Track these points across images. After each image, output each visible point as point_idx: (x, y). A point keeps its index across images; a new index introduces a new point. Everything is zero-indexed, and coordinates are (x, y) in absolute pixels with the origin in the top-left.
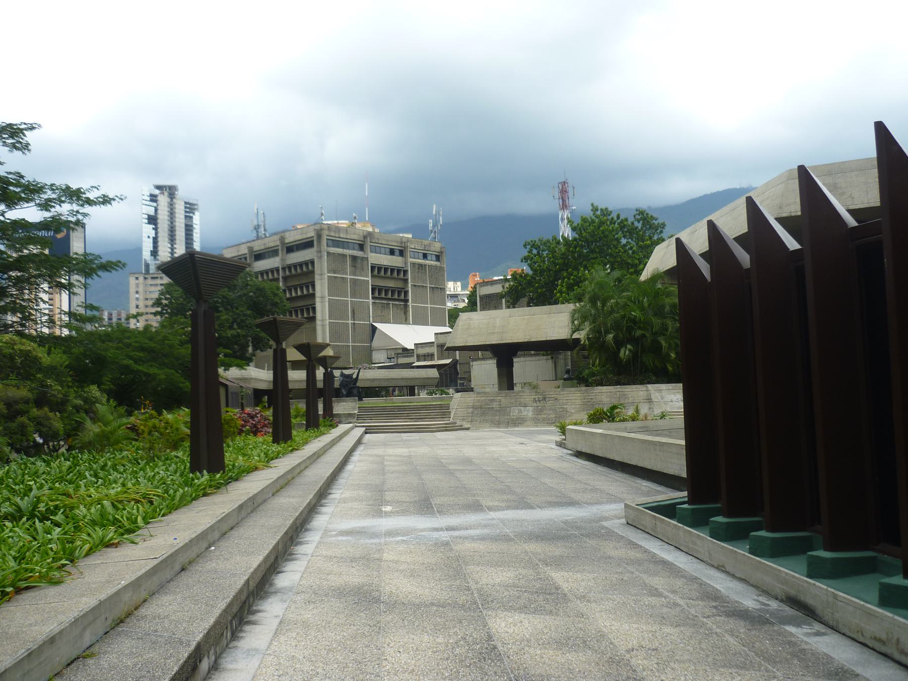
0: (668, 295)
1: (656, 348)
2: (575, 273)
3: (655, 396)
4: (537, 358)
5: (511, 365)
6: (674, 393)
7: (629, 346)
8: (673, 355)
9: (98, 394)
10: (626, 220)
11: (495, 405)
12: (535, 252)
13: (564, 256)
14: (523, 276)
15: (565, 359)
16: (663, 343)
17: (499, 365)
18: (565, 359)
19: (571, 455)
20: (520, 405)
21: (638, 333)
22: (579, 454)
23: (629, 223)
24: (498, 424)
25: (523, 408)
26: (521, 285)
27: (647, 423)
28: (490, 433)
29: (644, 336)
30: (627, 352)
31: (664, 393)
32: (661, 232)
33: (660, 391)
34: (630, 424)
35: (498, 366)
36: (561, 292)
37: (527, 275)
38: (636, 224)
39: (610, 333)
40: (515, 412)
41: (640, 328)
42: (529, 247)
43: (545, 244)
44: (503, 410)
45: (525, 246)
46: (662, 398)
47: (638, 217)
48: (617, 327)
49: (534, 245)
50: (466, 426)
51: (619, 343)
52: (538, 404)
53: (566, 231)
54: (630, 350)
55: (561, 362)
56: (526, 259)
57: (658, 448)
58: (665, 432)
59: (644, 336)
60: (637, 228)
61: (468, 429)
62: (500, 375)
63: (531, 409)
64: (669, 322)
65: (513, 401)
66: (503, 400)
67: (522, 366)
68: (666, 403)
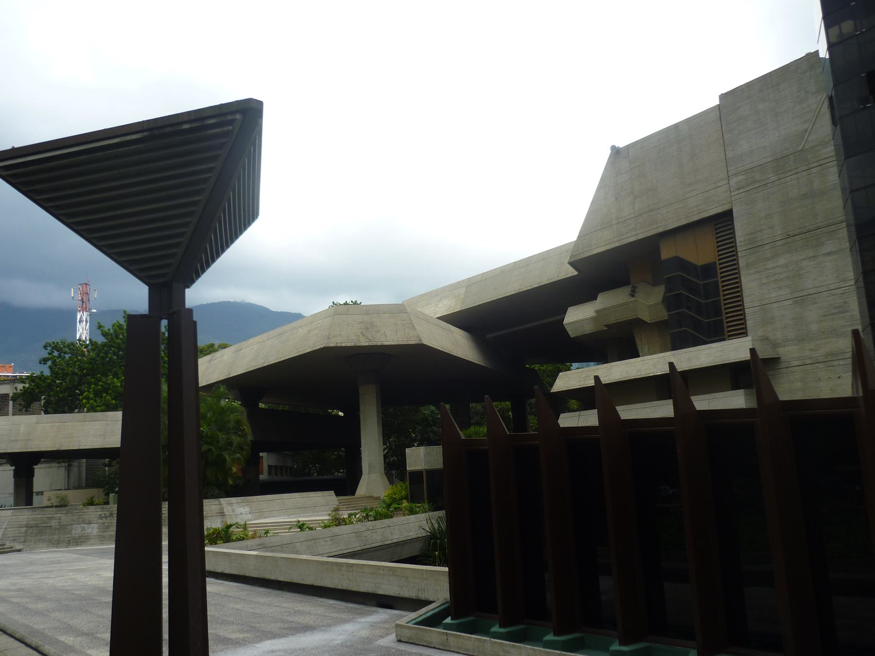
0: (233, 410)
1: (220, 463)
2: (104, 379)
3: (227, 510)
4: (48, 465)
5: (31, 474)
8: (234, 470)
11: (54, 523)
12: (56, 353)
13: (92, 361)
14: (41, 378)
15: (79, 467)
16: (227, 458)
17: (16, 475)
18: (79, 467)
20: (84, 522)
24: (57, 544)
25: (86, 526)
26: (38, 388)
27: (265, 540)
28: (49, 555)
29: (210, 450)
31: (235, 507)
33: (231, 504)
35: (14, 477)
36: (88, 398)
37: (47, 378)
40: (77, 530)
42: (49, 348)
43: (68, 346)
44: (62, 528)
45: (45, 347)
46: (233, 511)
49: (55, 347)
50: (18, 547)
52: (104, 520)
53: (83, 332)
55: (75, 470)
56: (44, 361)
57: (344, 568)
58: (278, 548)
59: (210, 450)
61: (19, 551)
62: (17, 486)
63: (96, 526)
65: (74, 518)
66: (64, 517)
67: (44, 477)
68: (236, 516)
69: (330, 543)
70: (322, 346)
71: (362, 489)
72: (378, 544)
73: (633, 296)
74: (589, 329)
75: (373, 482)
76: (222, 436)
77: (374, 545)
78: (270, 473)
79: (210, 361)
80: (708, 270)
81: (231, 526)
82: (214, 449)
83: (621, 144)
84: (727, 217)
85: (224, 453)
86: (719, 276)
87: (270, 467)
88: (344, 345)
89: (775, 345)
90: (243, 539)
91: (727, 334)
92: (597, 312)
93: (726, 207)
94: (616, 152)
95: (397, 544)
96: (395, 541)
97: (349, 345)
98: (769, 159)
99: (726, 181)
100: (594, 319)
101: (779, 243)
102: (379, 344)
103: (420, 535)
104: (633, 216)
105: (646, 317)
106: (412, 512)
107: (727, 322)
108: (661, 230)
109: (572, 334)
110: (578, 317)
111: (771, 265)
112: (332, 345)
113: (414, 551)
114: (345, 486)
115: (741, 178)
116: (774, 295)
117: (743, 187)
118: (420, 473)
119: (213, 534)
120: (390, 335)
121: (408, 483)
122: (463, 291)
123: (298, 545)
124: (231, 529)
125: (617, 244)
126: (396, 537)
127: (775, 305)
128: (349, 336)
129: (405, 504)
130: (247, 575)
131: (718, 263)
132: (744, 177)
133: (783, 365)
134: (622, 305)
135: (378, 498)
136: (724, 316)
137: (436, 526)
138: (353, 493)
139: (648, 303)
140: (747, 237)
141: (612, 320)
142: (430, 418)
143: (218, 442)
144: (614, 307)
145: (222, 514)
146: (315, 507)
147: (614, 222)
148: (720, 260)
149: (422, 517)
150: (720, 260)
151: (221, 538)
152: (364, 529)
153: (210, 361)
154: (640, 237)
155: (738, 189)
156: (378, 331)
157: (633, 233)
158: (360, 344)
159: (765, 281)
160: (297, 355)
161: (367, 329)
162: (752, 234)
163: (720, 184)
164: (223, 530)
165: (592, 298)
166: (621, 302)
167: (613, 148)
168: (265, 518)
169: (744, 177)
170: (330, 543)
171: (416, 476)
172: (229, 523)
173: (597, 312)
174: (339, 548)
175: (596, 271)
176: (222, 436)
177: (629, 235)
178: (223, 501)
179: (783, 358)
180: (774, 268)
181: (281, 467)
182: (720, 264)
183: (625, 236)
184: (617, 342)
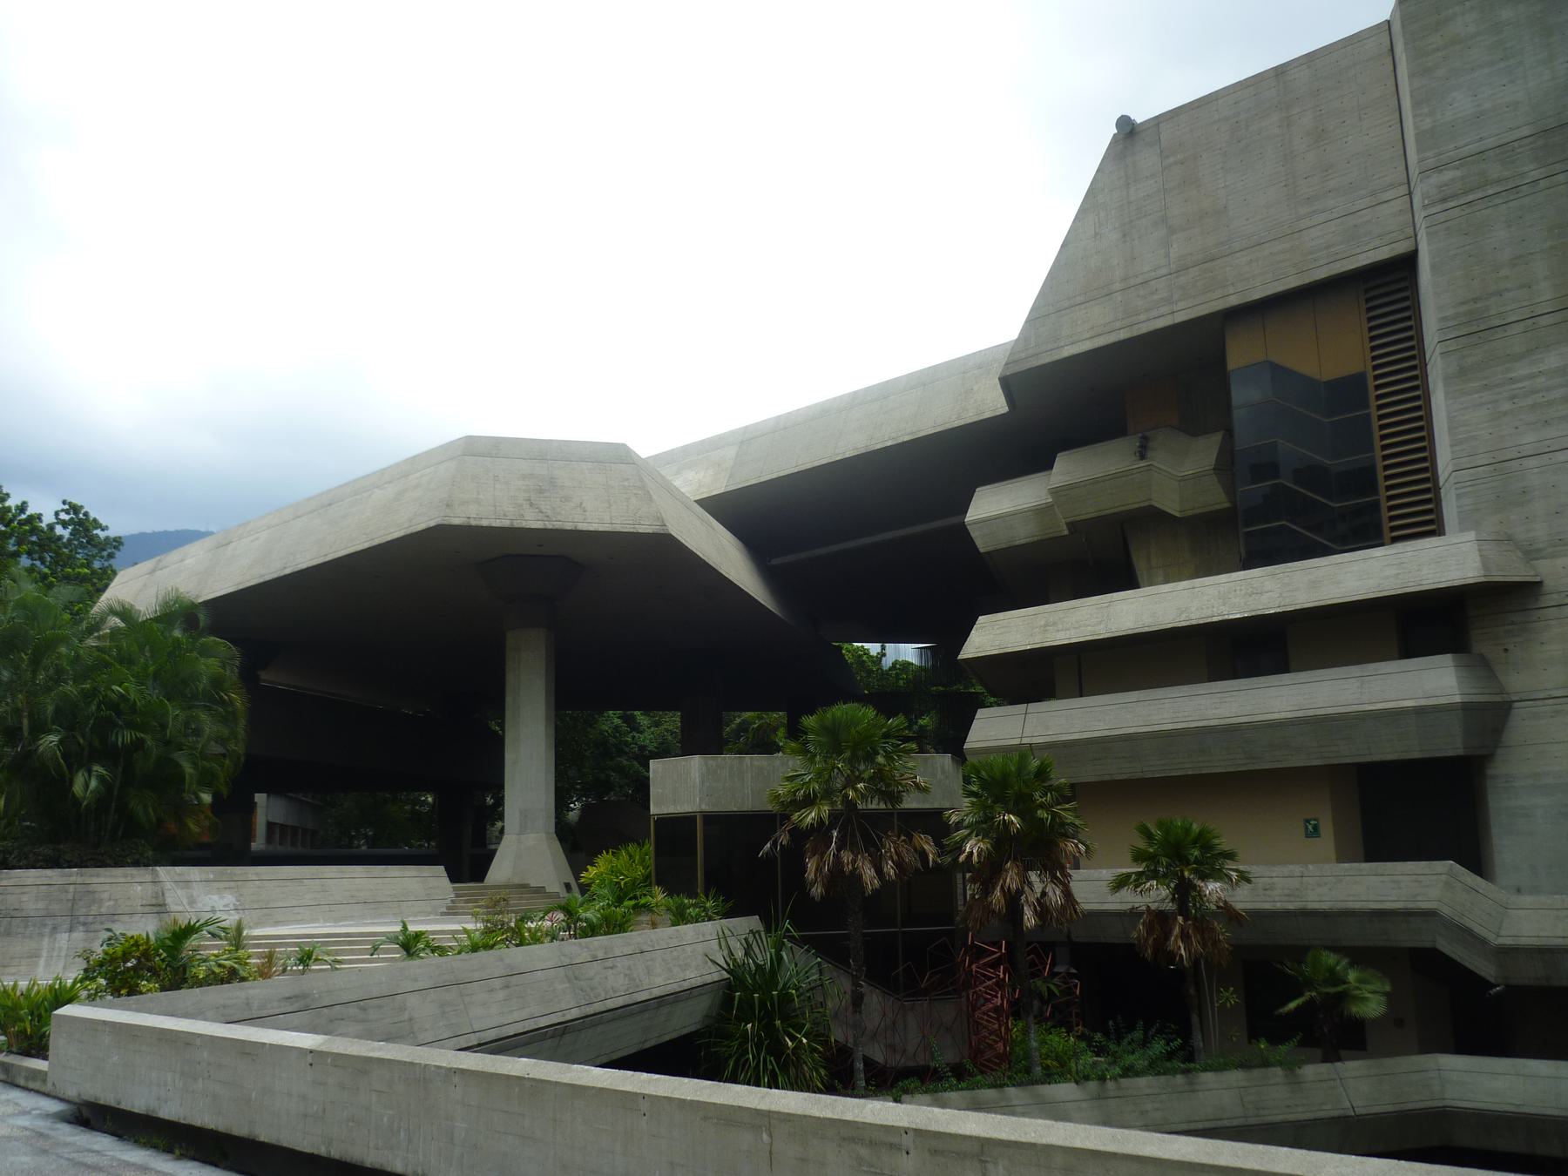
1: (166, 780)
6: (219, 891)
7: (98, 769)
9: (998, 892)
10: (39, 517)
16: (188, 768)
19: (62, 1118)
21: (125, 737)
22: (92, 1116)
23: (43, 525)
29: (139, 745)
30: (93, 783)
31: (197, 890)
32: (111, 556)
33: (187, 883)
34: (214, 994)
38: (59, 530)
39: (49, 732)
41: (131, 725)
47: (63, 516)
48: (68, 718)
51: (75, 758)
54: (101, 778)
59: (139, 745)
60: (60, 538)
64: (208, 725)
69: (501, 995)
70: (432, 524)
71: (500, 871)
72: (620, 1002)
73: (1142, 457)
74: (1023, 534)
75: (526, 849)
76: (174, 712)
77: (610, 1004)
78: (269, 838)
79: (153, 571)
80: (1349, 390)
81: (190, 930)
82: (150, 742)
83: (1139, 117)
84: (1399, 273)
85: (176, 755)
86: (1374, 403)
87: (271, 826)
88: (485, 523)
89: (1530, 553)
90: (232, 976)
91: (1387, 535)
92: (1055, 492)
93: (1402, 248)
94: (1128, 131)
95: (661, 1001)
96: (657, 992)
97: (497, 524)
98: (1526, 131)
99: (1403, 190)
100: (1041, 512)
101: (1544, 321)
102: (568, 526)
103: (709, 979)
104: (1164, 271)
105: (1172, 505)
106: (680, 917)
107: (1391, 508)
108: (1234, 301)
109: (983, 544)
110: (999, 509)
111: (1522, 369)
112: (456, 521)
113: (682, 1022)
114: (466, 856)
115: (1449, 175)
116: (1529, 438)
117: (1454, 196)
118: (687, 820)
119: (125, 957)
120: (594, 511)
121: (650, 847)
122: (731, 452)
123: (413, 1000)
124: (193, 942)
125: (1123, 335)
126: (659, 981)
127: (1532, 462)
128: (494, 506)
129: (659, 896)
130: (264, 1136)
131: (1371, 374)
132: (1458, 173)
133: (1546, 601)
134: (1116, 476)
135: (540, 891)
136: (1383, 494)
137: (739, 954)
138: (482, 880)
139: (1179, 474)
140: (1463, 309)
141: (1087, 511)
142: (612, 740)
143: (164, 727)
144: (1095, 481)
145: (159, 907)
146: (413, 897)
147: (1117, 286)
148: (1375, 368)
149: (709, 928)
150: (1375, 368)
151: (155, 972)
152: (585, 956)
153: (153, 571)
154: (1180, 317)
155: (1444, 200)
156: (567, 499)
157: (1165, 310)
158: (524, 525)
159: (1507, 406)
160: (366, 545)
161: (541, 491)
162: (1475, 300)
163: (1386, 196)
164: (161, 942)
165: (1047, 465)
166: (1113, 469)
167: (1125, 124)
168: (277, 923)
169: (1458, 173)
170: (501, 995)
171: (676, 830)
172: (183, 923)
173: (1055, 492)
174: (524, 1014)
175: (1057, 403)
176: (174, 712)
177: (1154, 313)
178: (163, 872)
179: (1549, 584)
180: (1531, 377)
181: (295, 829)
182: (1376, 377)
183: (1143, 317)
184: (1095, 556)
